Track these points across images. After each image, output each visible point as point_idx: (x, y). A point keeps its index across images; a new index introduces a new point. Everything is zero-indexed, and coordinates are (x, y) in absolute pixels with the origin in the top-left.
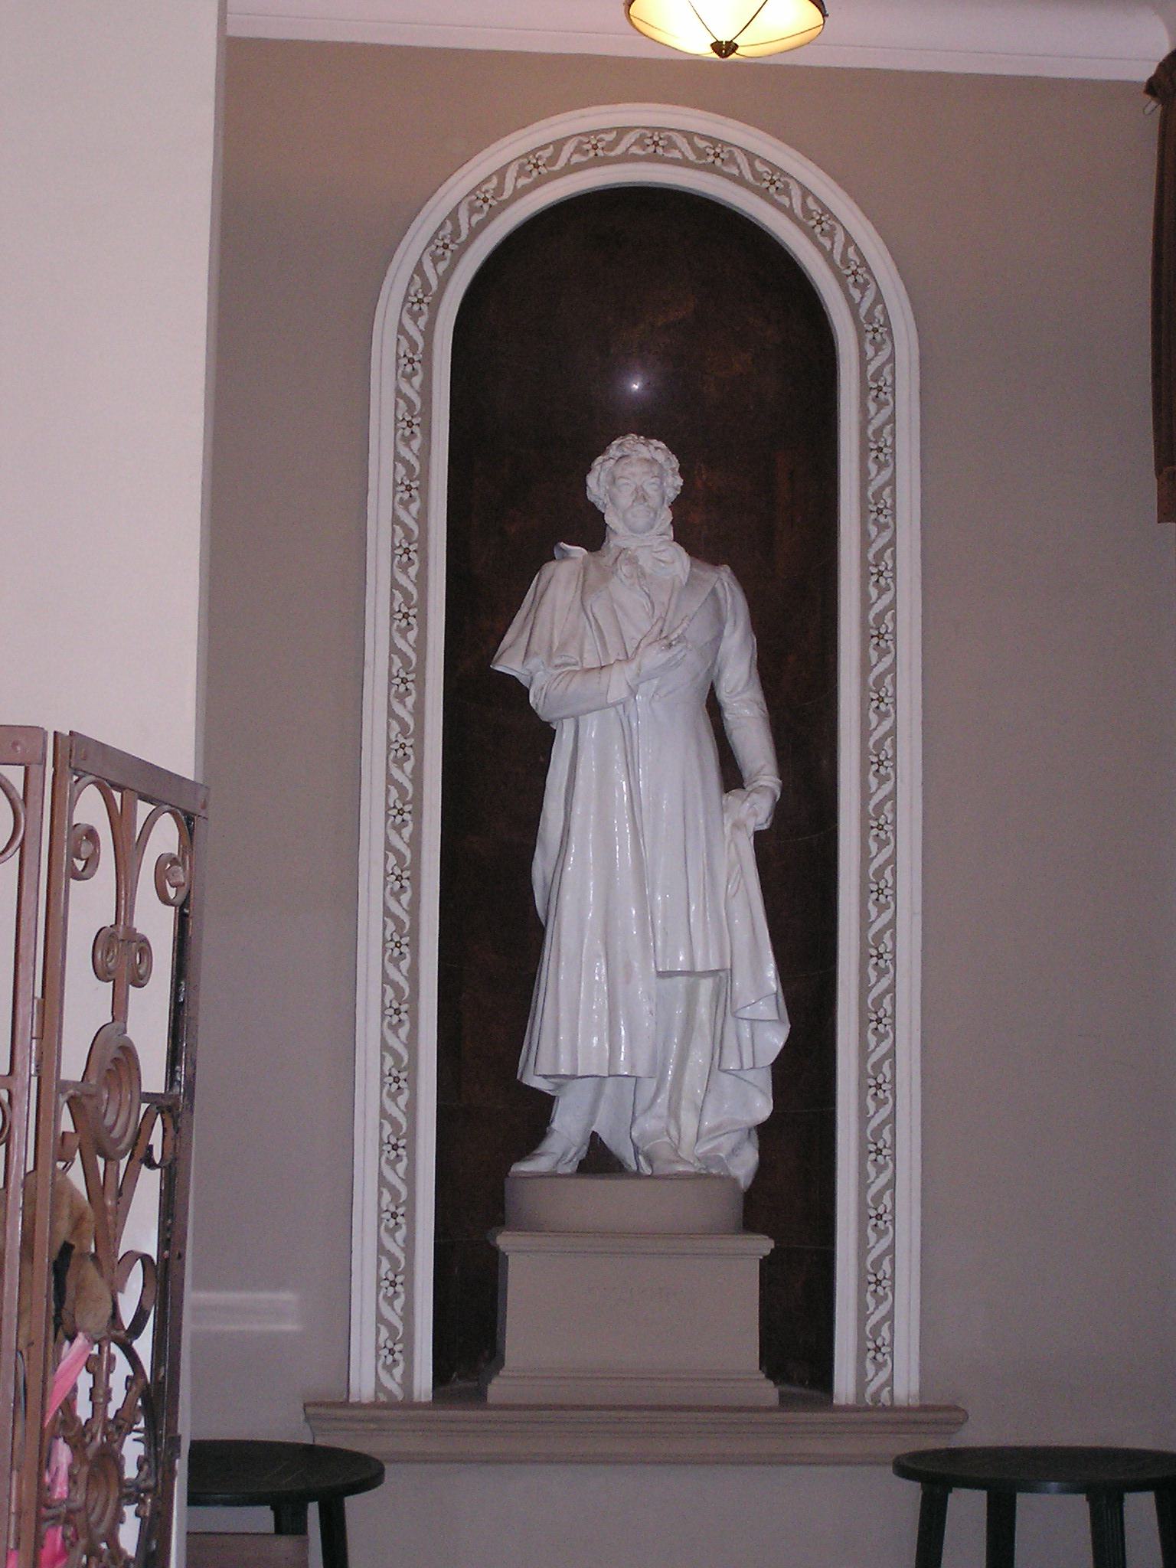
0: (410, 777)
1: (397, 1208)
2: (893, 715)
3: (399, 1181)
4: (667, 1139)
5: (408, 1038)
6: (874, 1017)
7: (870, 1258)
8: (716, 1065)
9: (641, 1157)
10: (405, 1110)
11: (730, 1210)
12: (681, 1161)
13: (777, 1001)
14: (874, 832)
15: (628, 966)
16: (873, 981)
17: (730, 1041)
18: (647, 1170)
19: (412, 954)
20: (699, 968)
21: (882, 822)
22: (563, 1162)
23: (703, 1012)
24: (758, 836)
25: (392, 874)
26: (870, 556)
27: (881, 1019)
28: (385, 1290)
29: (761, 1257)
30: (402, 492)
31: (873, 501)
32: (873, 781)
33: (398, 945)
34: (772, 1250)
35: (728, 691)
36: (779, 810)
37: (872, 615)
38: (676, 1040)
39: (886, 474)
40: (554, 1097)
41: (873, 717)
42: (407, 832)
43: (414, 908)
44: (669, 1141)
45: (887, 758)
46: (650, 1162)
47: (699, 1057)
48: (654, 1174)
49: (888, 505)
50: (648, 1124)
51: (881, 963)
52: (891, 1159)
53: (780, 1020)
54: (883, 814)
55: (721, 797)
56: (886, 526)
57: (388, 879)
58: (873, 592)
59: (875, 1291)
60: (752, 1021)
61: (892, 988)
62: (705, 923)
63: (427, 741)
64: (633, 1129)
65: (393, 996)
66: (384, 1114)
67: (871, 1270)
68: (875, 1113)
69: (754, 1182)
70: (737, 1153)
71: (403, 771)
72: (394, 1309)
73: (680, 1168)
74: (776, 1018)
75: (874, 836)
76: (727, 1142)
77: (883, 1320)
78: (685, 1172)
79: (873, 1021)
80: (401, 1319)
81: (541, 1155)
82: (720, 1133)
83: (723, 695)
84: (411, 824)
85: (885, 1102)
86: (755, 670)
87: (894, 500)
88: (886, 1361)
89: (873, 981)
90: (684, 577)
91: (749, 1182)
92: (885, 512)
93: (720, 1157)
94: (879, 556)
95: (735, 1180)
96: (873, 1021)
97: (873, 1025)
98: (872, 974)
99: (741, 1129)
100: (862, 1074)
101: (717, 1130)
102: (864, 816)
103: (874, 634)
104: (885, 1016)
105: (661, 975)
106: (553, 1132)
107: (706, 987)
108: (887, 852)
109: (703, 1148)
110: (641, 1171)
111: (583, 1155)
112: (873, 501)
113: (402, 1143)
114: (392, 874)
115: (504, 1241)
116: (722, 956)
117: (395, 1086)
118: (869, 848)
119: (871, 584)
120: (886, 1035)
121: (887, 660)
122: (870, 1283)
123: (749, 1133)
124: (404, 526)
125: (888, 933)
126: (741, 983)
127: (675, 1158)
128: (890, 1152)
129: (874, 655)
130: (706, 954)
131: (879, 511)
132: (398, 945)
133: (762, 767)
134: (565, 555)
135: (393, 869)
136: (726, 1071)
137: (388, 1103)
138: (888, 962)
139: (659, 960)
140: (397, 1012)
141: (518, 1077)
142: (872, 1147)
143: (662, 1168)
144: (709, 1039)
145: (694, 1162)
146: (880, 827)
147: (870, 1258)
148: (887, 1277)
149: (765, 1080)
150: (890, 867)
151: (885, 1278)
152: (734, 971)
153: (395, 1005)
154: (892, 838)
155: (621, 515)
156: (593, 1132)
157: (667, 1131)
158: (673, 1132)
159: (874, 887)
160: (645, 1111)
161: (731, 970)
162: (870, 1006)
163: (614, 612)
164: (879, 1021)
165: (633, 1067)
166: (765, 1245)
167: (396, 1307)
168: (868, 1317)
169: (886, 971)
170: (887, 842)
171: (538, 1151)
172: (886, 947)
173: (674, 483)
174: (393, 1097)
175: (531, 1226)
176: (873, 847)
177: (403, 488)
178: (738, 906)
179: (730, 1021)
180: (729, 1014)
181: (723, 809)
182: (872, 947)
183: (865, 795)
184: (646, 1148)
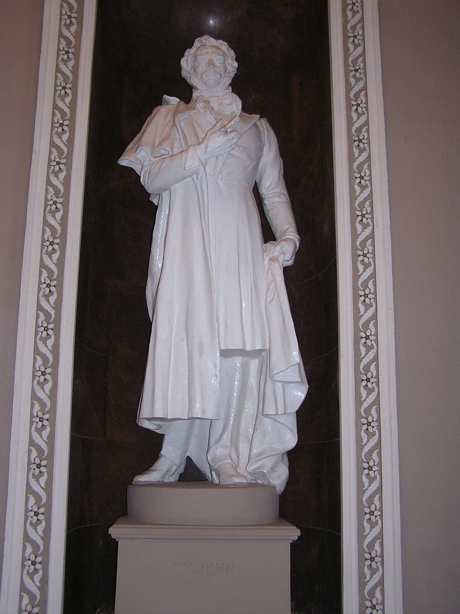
0: (60, 222)
1: (39, 508)
2: (370, 187)
3: (42, 490)
4: (230, 461)
5: (50, 391)
6: (364, 378)
7: (359, 241)
8: (261, 413)
9: (213, 473)
10: (47, 441)
11: (273, 508)
12: (239, 475)
13: (300, 369)
14: (361, 258)
15: (201, 344)
16: (363, 354)
17: (269, 395)
18: (216, 481)
19: (73, 94)
20: (249, 348)
21: (365, 252)
22: (169, 475)
23: (253, 381)
24: (286, 270)
25: (44, 283)
26: (352, 95)
27: (369, 379)
28: (28, 568)
29: (292, 542)
30: (63, 54)
31: (352, 65)
32: (359, 227)
33: (46, 329)
34: (299, 537)
35: (266, 188)
36: (298, 255)
37: (354, 129)
38: (235, 394)
39: (359, 50)
40: (162, 436)
41: (358, 189)
42: (56, 256)
43: (58, 306)
44: (231, 462)
45: (367, 213)
46: (218, 475)
47: (250, 408)
48: (221, 483)
49: (361, 67)
50: (218, 451)
51: (368, 342)
52: (378, 473)
53: (302, 382)
54: (366, 247)
55: (262, 245)
56: (361, 79)
57: (41, 286)
58: (354, 116)
59: (370, 565)
60: (284, 382)
61: (376, 359)
62: (252, 319)
63: (72, 200)
64: (208, 454)
65: (41, 363)
66: (32, 442)
67: (367, 551)
68: (367, 442)
69: (286, 488)
70: (275, 470)
71: (55, 219)
72: (33, 581)
73: (237, 480)
74: (299, 380)
75: (361, 261)
76: (268, 463)
77: (372, 361)
78: (240, 483)
79: (364, 380)
80: (39, 588)
81: (152, 470)
82: (264, 456)
83: (264, 191)
84: (58, 251)
85: (373, 434)
86: (282, 177)
87: (365, 65)
88: (377, 521)
89: (363, 354)
90: (238, 113)
91: (282, 489)
92: (359, 71)
93: (264, 473)
94: (357, 95)
95: (273, 488)
96: (364, 380)
97: (364, 383)
98: (363, 349)
99: (277, 454)
100: (361, 551)
101: (261, 455)
102: (354, 248)
103: (356, 139)
104: (372, 377)
105: (226, 353)
106: (162, 457)
107: (254, 364)
108: (370, 271)
109: (251, 468)
110: (214, 482)
111: (181, 470)
112: (352, 65)
113: (44, 463)
114: (44, 283)
115: (114, 531)
116: (264, 341)
117: (40, 424)
118: (360, 393)
119: (358, 221)
120: (373, 390)
121: (365, 155)
122: (366, 559)
123: (282, 457)
124: (63, 74)
125: (372, 322)
126: (276, 356)
127: (236, 474)
128: (377, 468)
129: (356, 152)
130: (253, 340)
131: (356, 71)
132: (46, 329)
133: (288, 228)
134: (167, 103)
135: (45, 280)
136: (266, 416)
137: (35, 435)
138: (373, 341)
139: (222, 344)
140: (44, 373)
141: (137, 422)
142: (365, 465)
143: (226, 481)
144: (257, 397)
145: (247, 476)
146: (365, 255)
147: (359, 241)
148: (378, 555)
149: (292, 422)
150: (371, 281)
151: (370, 293)
152: (271, 350)
153: (43, 369)
154: (372, 262)
155: (200, 77)
156: (188, 456)
157: (230, 455)
158: (234, 456)
159: (362, 293)
160: (216, 443)
161: (270, 350)
162: (362, 371)
163: (193, 126)
164: (368, 380)
165: (204, 412)
166: (294, 533)
167: (38, 530)
168: (366, 584)
169: (372, 347)
170: (369, 265)
171: (152, 468)
172: (371, 332)
173: (233, 66)
174: (39, 431)
175: (139, 521)
176: (361, 267)
177: (64, 52)
178: (274, 308)
179: (269, 383)
180: (268, 378)
181: (264, 251)
182: (362, 331)
183: (357, 316)
184: (216, 467)
